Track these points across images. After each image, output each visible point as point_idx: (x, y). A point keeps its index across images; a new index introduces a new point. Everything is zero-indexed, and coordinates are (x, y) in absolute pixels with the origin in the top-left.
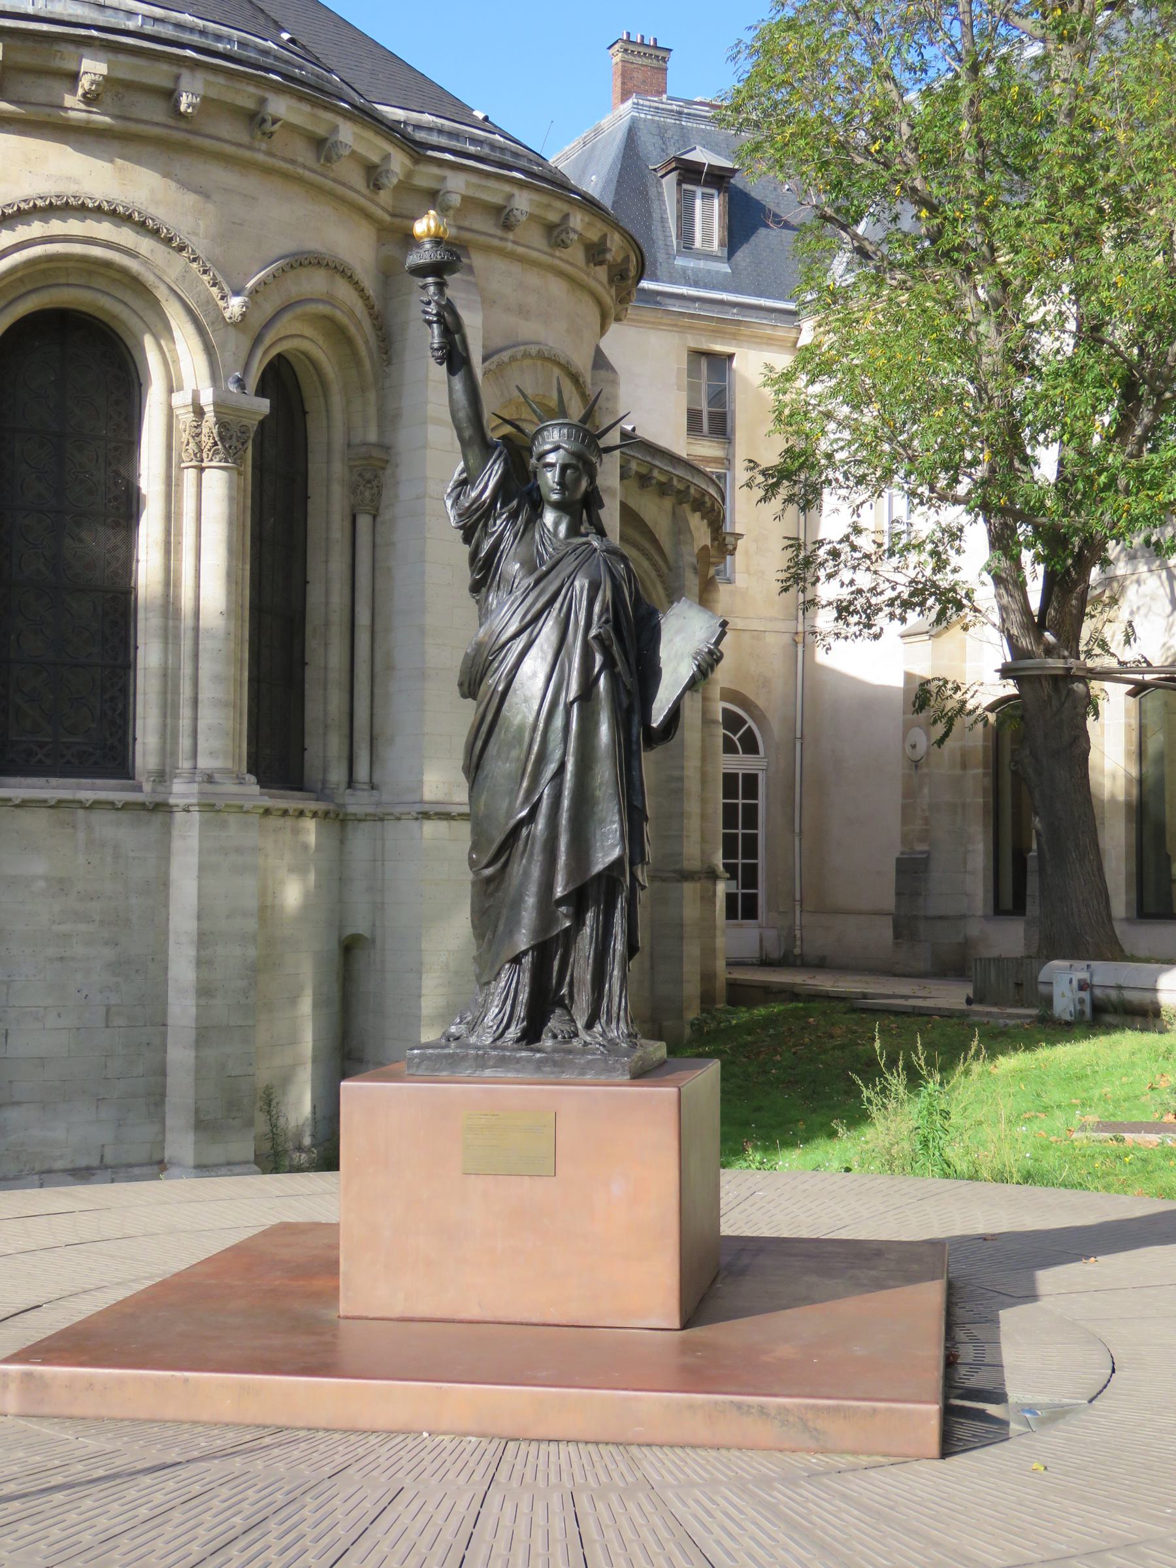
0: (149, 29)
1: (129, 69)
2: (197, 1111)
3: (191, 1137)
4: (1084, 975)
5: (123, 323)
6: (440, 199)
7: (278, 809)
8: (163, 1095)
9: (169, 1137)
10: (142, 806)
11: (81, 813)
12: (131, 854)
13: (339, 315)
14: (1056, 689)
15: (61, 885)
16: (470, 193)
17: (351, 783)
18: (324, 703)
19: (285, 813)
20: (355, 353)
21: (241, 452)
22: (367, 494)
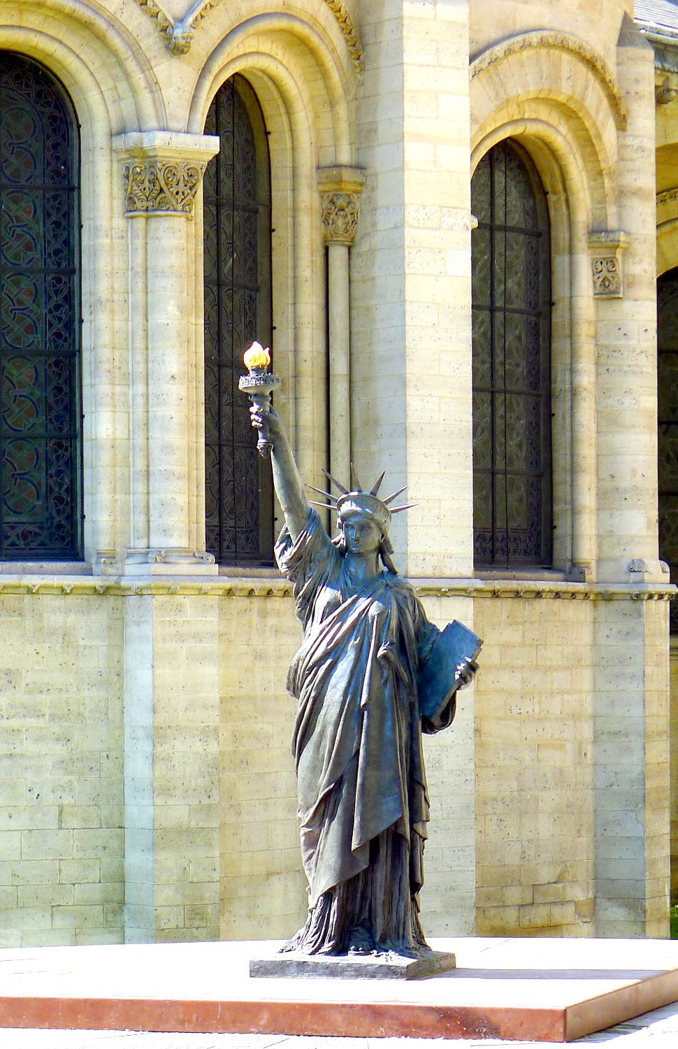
7: (242, 589)
8: (122, 903)
12: (82, 643)
13: (298, 27)
20: (320, 65)
21: (190, 197)
22: (340, 222)
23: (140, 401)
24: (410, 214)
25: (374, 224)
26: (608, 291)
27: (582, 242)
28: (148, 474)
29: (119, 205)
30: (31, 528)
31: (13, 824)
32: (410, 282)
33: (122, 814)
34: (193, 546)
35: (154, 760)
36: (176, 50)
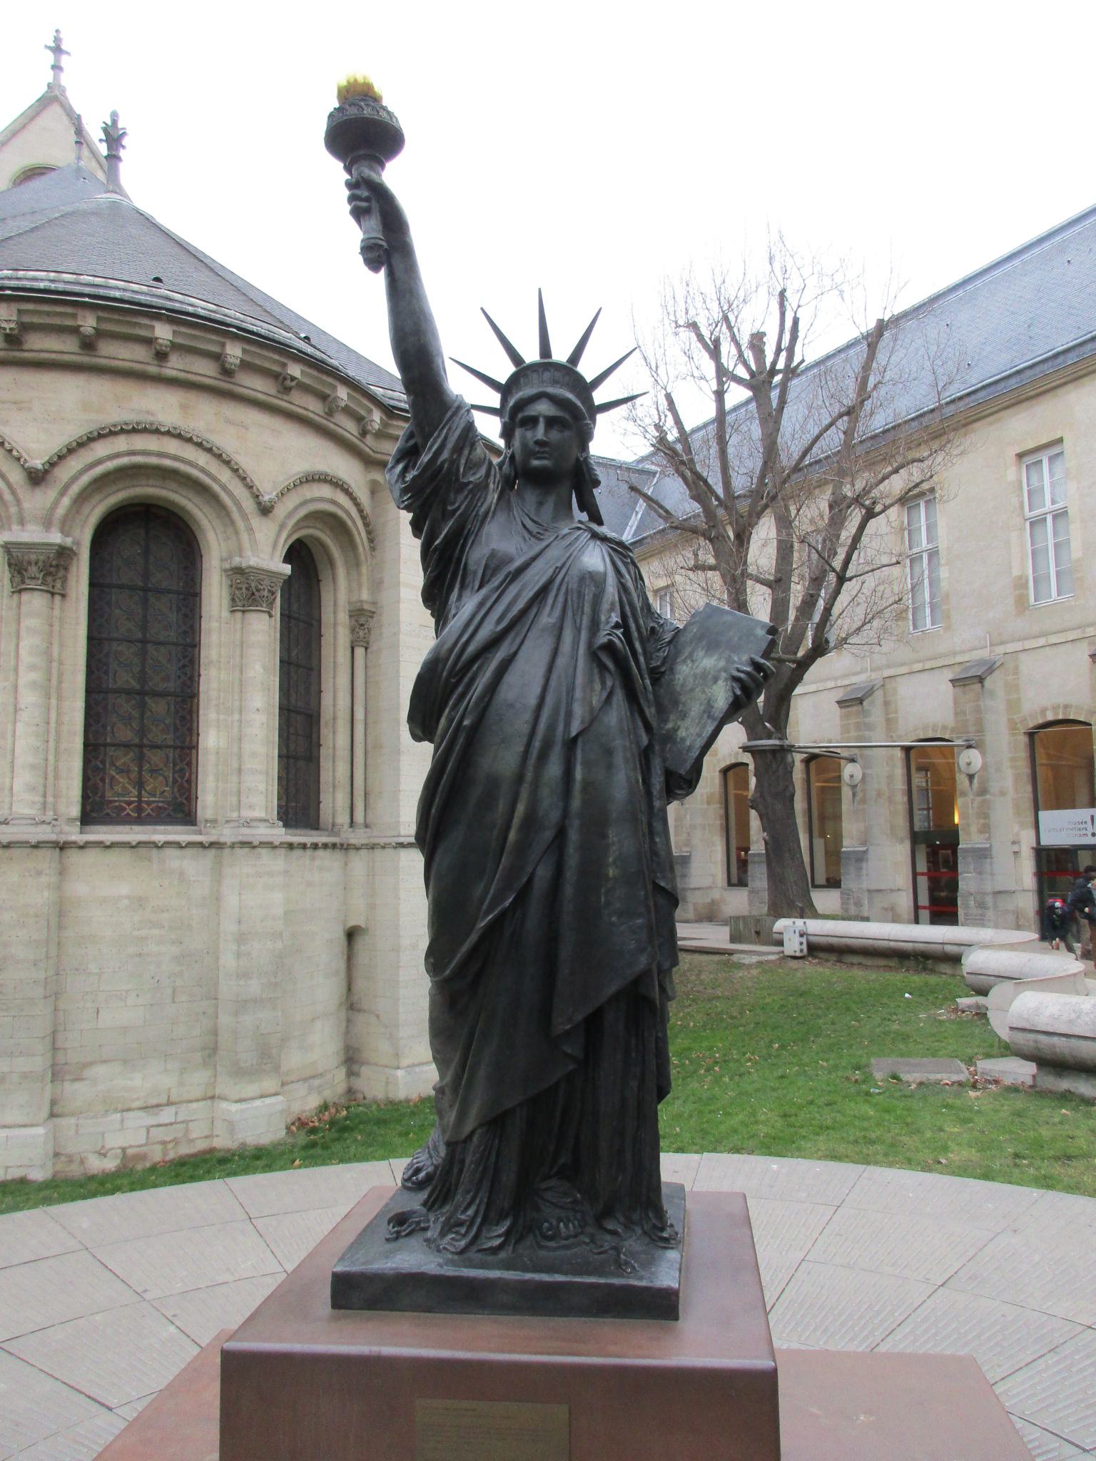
5: (188, 512)
10: (201, 845)
11: (155, 851)
14: (774, 757)
15: (139, 902)
17: (352, 824)
19: (304, 846)
23: (236, 724)
24: (403, 627)
25: (381, 634)
28: (240, 770)
29: (226, 602)
32: (402, 665)
34: (268, 817)
35: (239, 955)
36: (265, 510)
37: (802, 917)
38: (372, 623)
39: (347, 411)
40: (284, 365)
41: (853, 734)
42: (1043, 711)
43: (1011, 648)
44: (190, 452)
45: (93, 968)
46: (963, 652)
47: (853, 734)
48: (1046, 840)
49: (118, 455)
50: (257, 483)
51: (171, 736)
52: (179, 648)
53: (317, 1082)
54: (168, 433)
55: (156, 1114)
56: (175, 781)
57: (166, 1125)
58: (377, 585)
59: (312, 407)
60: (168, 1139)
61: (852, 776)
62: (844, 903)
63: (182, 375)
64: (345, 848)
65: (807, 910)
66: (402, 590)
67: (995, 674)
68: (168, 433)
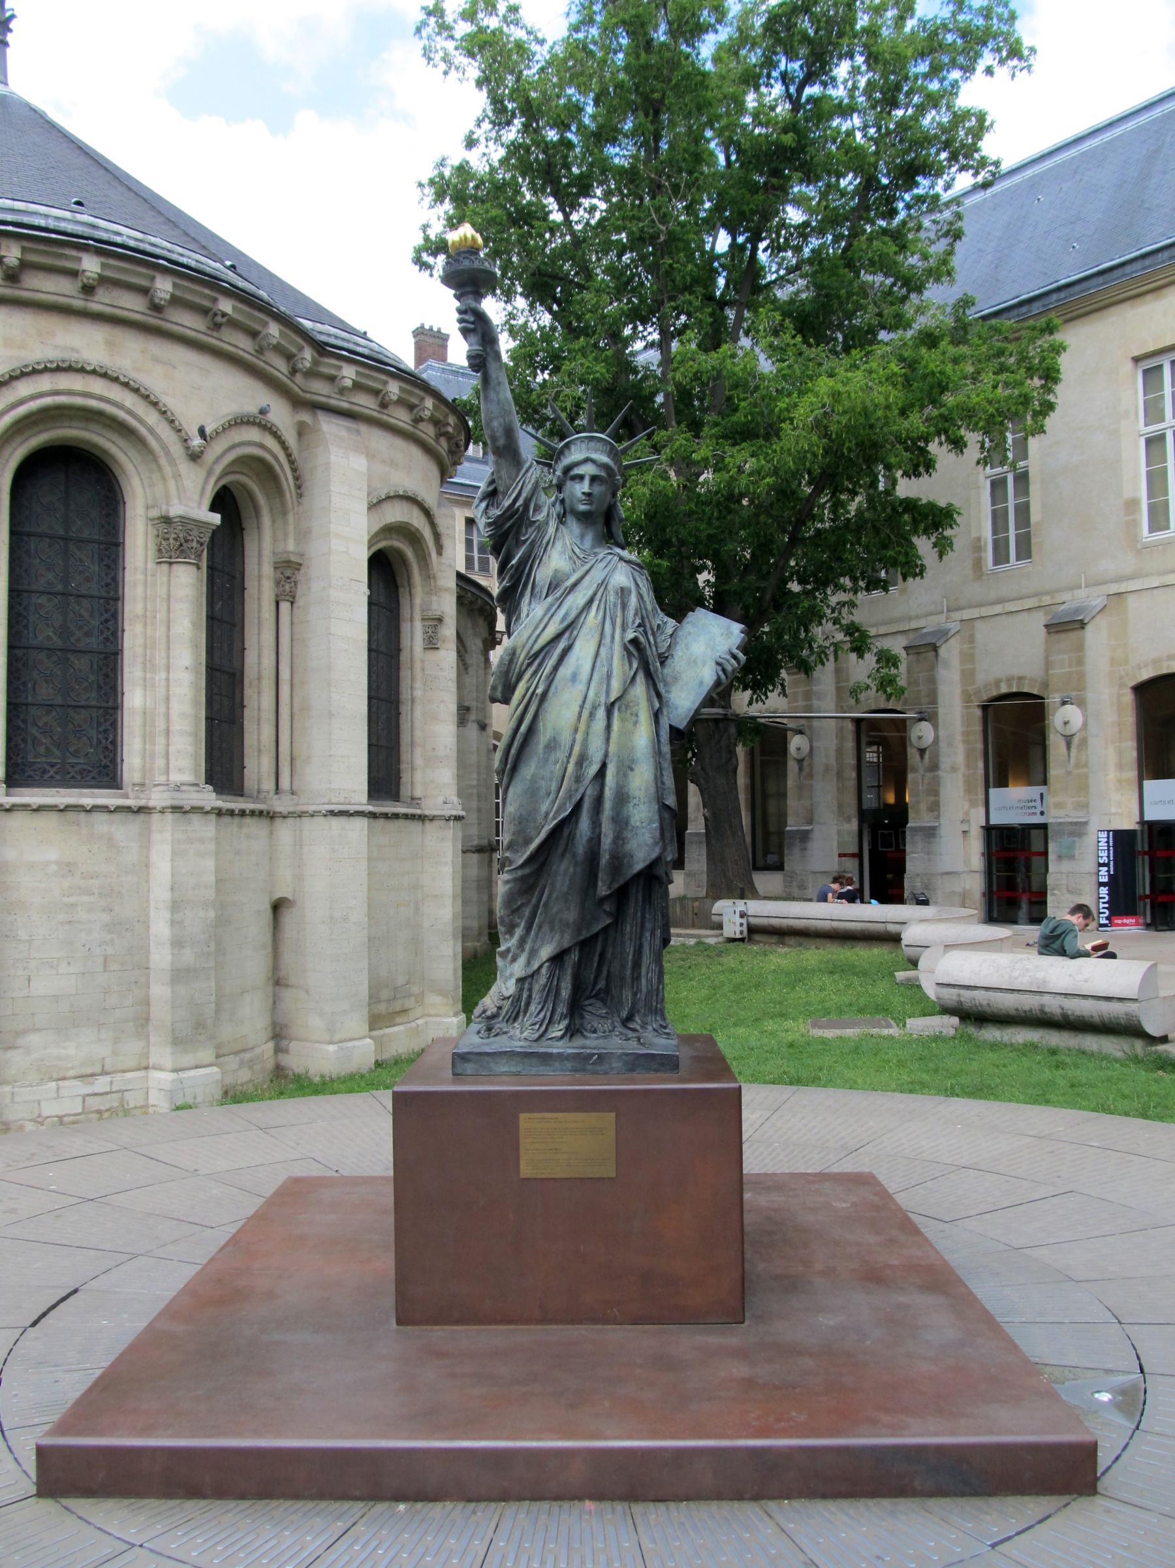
0: (132, 243)
1: (119, 270)
2: (173, 1030)
3: (169, 1049)
4: (743, 908)
5: (112, 457)
6: (337, 381)
8: (148, 1019)
9: (153, 1049)
10: (128, 809)
11: (83, 815)
15: (68, 868)
16: (359, 379)
18: (257, 734)
25: (309, 588)
26: (432, 645)
27: (417, 616)
29: (152, 553)
30: (85, 767)
31: (72, 969)
33: (148, 960)
37: (742, 898)
38: (300, 576)
39: (278, 349)
40: (215, 300)
41: (801, 703)
42: (998, 683)
43: (967, 614)
44: (116, 393)
45: (23, 934)
46: (918, 617)
47: (801, 703)
48: (994, 821)
49: (41, 395)
50: (185, 426)
51: (94, 694)
52: (102, 601)
53: (247, 1056)
54: (94, 372)
55: (92, 1084)
56: (99, 742)
57: (102, 1094)
58: (303, 535)
59: (241, 344)
60: (103, 1108)
61: (799, 749)
62: (788, 882)
63: (108, 310)
64: (270, 816)
65: (746, 891)
66: (333, 541)
67: (952, 641)
68: (94, 372)
